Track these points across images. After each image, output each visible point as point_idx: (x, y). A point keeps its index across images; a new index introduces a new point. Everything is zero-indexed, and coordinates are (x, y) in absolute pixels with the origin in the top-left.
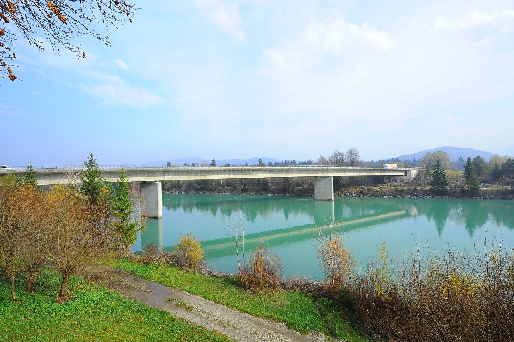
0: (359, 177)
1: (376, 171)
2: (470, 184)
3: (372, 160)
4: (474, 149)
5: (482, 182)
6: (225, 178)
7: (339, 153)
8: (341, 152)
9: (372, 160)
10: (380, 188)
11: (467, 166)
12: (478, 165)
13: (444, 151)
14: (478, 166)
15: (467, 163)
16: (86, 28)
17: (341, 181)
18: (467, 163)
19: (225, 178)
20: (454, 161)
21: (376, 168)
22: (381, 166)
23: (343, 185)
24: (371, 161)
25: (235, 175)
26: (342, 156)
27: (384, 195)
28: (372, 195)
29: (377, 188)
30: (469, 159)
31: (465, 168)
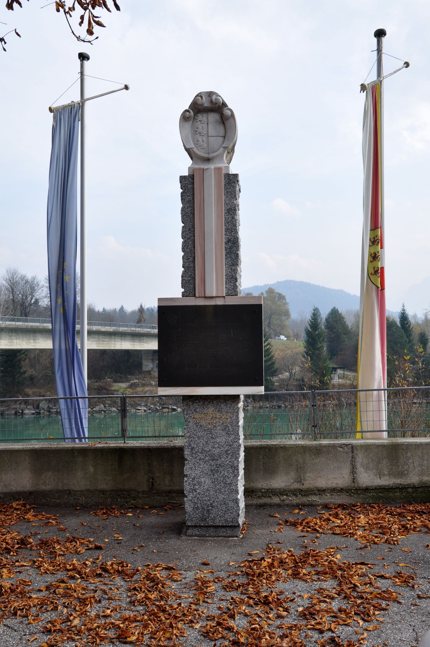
0: (48, 350)
1: (123, 335)
2: (315, 371)
3: (122, 308)
4: (276, 282)
5: (340, 368)
6: (121, 347)
7: (23, 278)
8: (29, 276)
9: (122, 308)
10: (131, 386)
11: (310, 330)
12: (335, 328)
13: (280, 292)
14: (334, 330)
15: (310, 321)
16: (73, 32)
17: (25, 366)
18: (310, 321)
19: (121, 347)
20: (303, 319)
21: (121, 329)
22: (138, 322)
23: (32, 378)
24: (118, 308)
25: (134, 342)
26: (33, 289)
27: (140, 405)
28: (110, 405)
29: (123, 385)
30: (315, 315)
31: (308, 333)
